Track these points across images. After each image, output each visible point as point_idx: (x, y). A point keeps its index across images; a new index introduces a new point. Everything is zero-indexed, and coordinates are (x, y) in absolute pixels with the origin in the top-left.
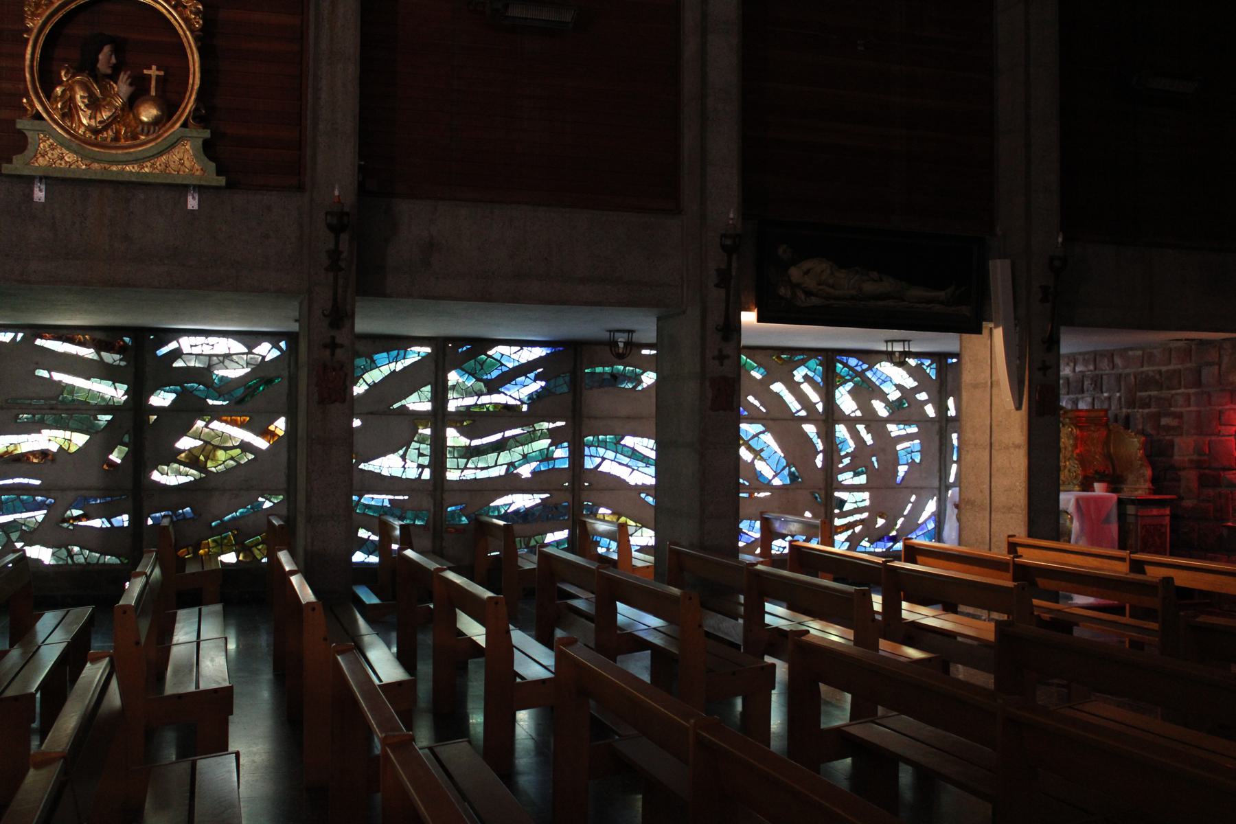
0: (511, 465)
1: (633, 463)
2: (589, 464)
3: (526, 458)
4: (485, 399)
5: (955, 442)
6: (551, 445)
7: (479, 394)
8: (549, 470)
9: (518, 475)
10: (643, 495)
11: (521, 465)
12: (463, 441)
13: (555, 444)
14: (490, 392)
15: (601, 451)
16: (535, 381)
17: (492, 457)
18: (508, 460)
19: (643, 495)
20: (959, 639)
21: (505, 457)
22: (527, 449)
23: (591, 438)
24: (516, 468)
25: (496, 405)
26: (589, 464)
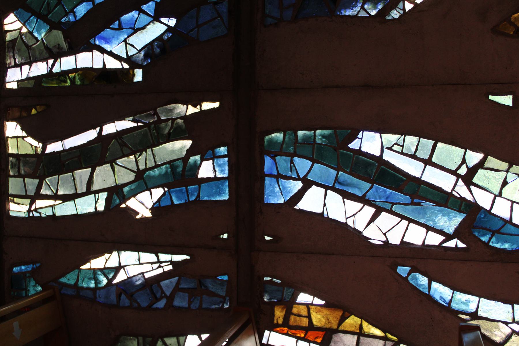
0: (116, 193)
1: (379, 193)
2: (276, 195)
3: (142, 181)
4: (67, 63)
5: (269, 279)
6: (191, 152)
7: (56, 54)
8: (188, 203)
9: (131, 212)
10: (403, 270)
11: (134, 194)
12: (31, 144)
13: (203, 149)
14: (73, 51)
15: (303, 165)
16: (156, 18)
17: (83, 174)
18: (110, 183)
19: (403, 270)
20: (171, 131)
21: (104, 176)
22: (145, 160)
23: (278, 136)
24: (125, 199)
25: (86, 72)
26: (276, 195)
